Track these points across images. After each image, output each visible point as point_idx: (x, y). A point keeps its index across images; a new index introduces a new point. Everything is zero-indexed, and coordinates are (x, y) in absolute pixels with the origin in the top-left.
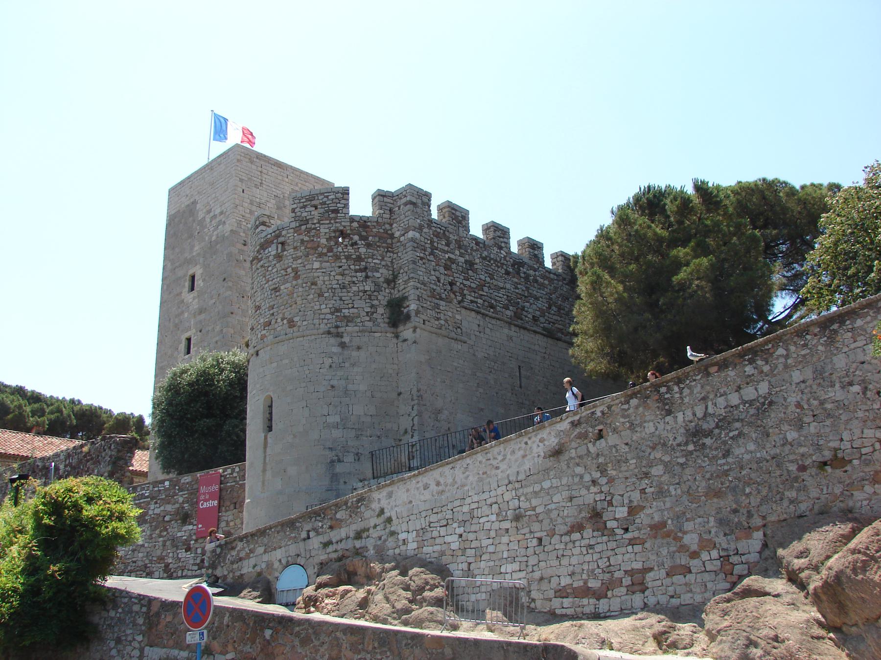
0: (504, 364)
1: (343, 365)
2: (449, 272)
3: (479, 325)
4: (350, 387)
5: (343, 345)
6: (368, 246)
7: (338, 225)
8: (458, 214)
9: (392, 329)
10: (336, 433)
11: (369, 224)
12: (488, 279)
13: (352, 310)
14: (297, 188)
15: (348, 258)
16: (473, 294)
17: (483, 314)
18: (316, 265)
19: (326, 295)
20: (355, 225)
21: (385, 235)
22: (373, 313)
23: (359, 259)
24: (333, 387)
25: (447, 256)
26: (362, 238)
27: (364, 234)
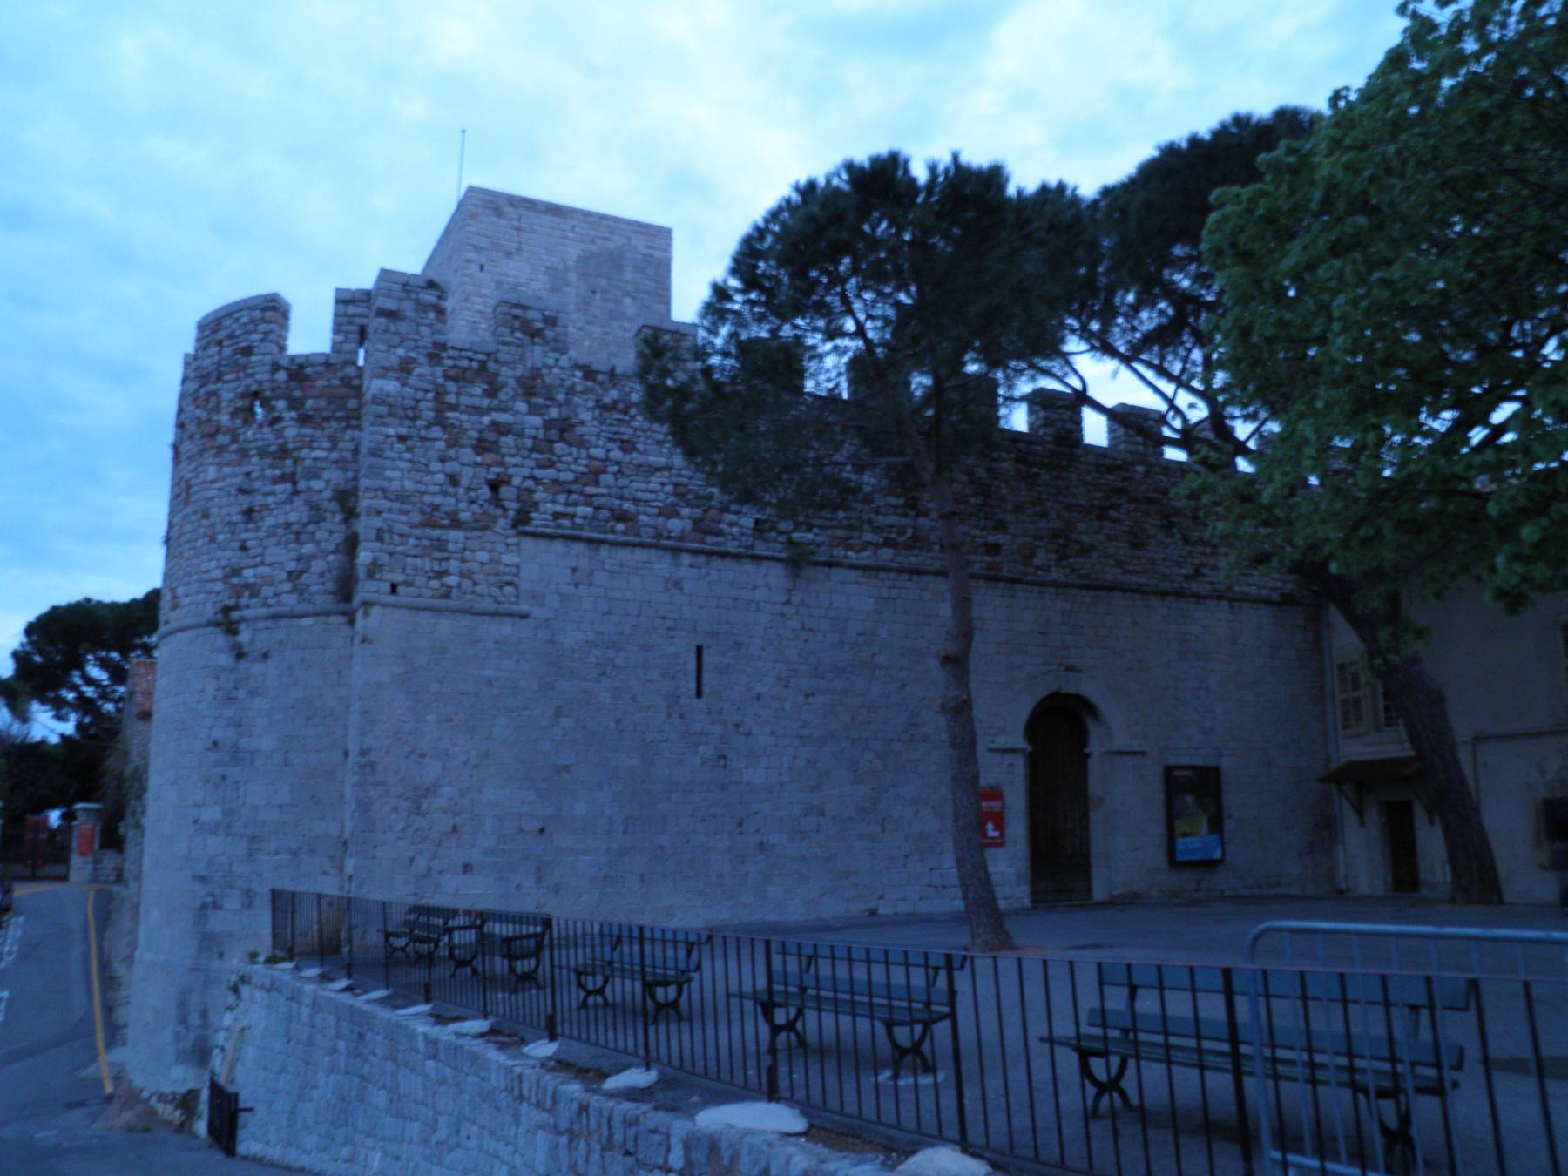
0: (646, 648)
1: (234, 694)
2: (489, 457)
3: (574, 570)
4: (244, 741)
5: (240, 654)
6: (304, 420)
7: (249, 381)
8: (531, 314)
9: (341, 607)
10: (215, 844)
11: (308, 370)
12: (616, 454)
13: (261, 570)
14: (594, 248)
15: (263, 453)
16: (562, 498)
17: (590, 541)
18: (212, 472)
19: (220, 537)
20: (281, 376)
21: (344, 391)
22: (301, 573)
23: (283, 452)
24: (215, 744)
25: (486, 420)
26: (294, 404)
27: (297, 393)
